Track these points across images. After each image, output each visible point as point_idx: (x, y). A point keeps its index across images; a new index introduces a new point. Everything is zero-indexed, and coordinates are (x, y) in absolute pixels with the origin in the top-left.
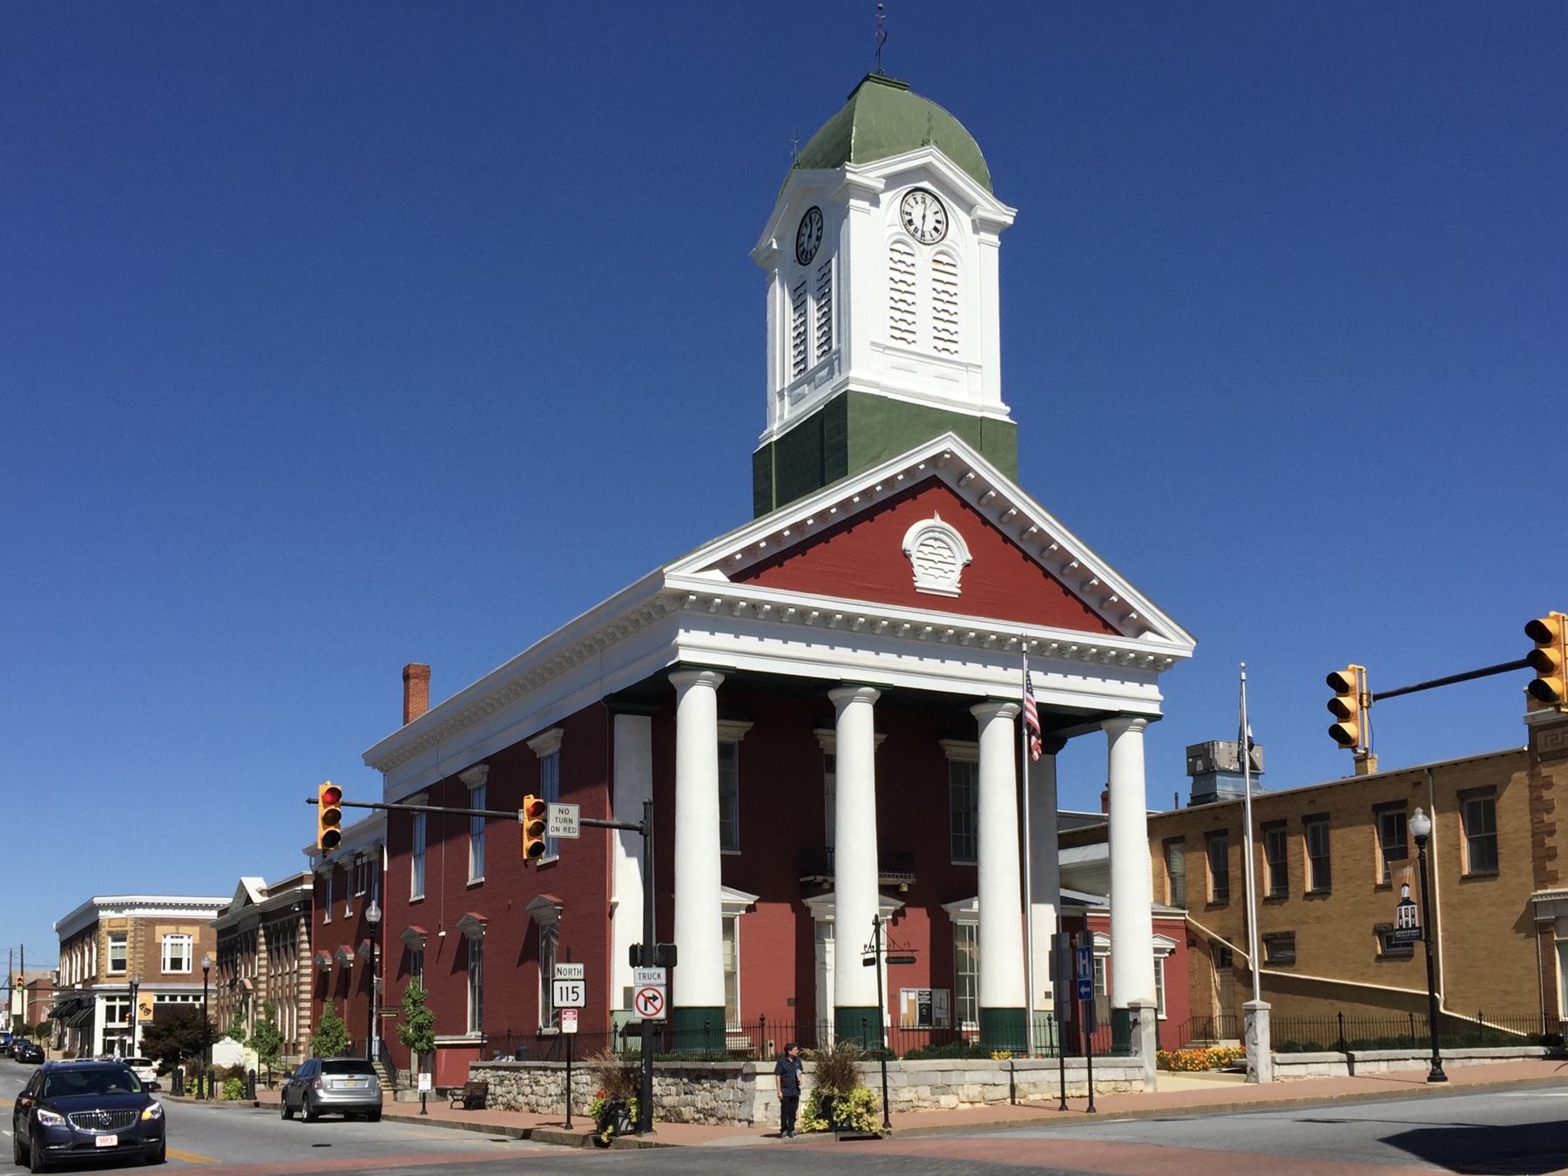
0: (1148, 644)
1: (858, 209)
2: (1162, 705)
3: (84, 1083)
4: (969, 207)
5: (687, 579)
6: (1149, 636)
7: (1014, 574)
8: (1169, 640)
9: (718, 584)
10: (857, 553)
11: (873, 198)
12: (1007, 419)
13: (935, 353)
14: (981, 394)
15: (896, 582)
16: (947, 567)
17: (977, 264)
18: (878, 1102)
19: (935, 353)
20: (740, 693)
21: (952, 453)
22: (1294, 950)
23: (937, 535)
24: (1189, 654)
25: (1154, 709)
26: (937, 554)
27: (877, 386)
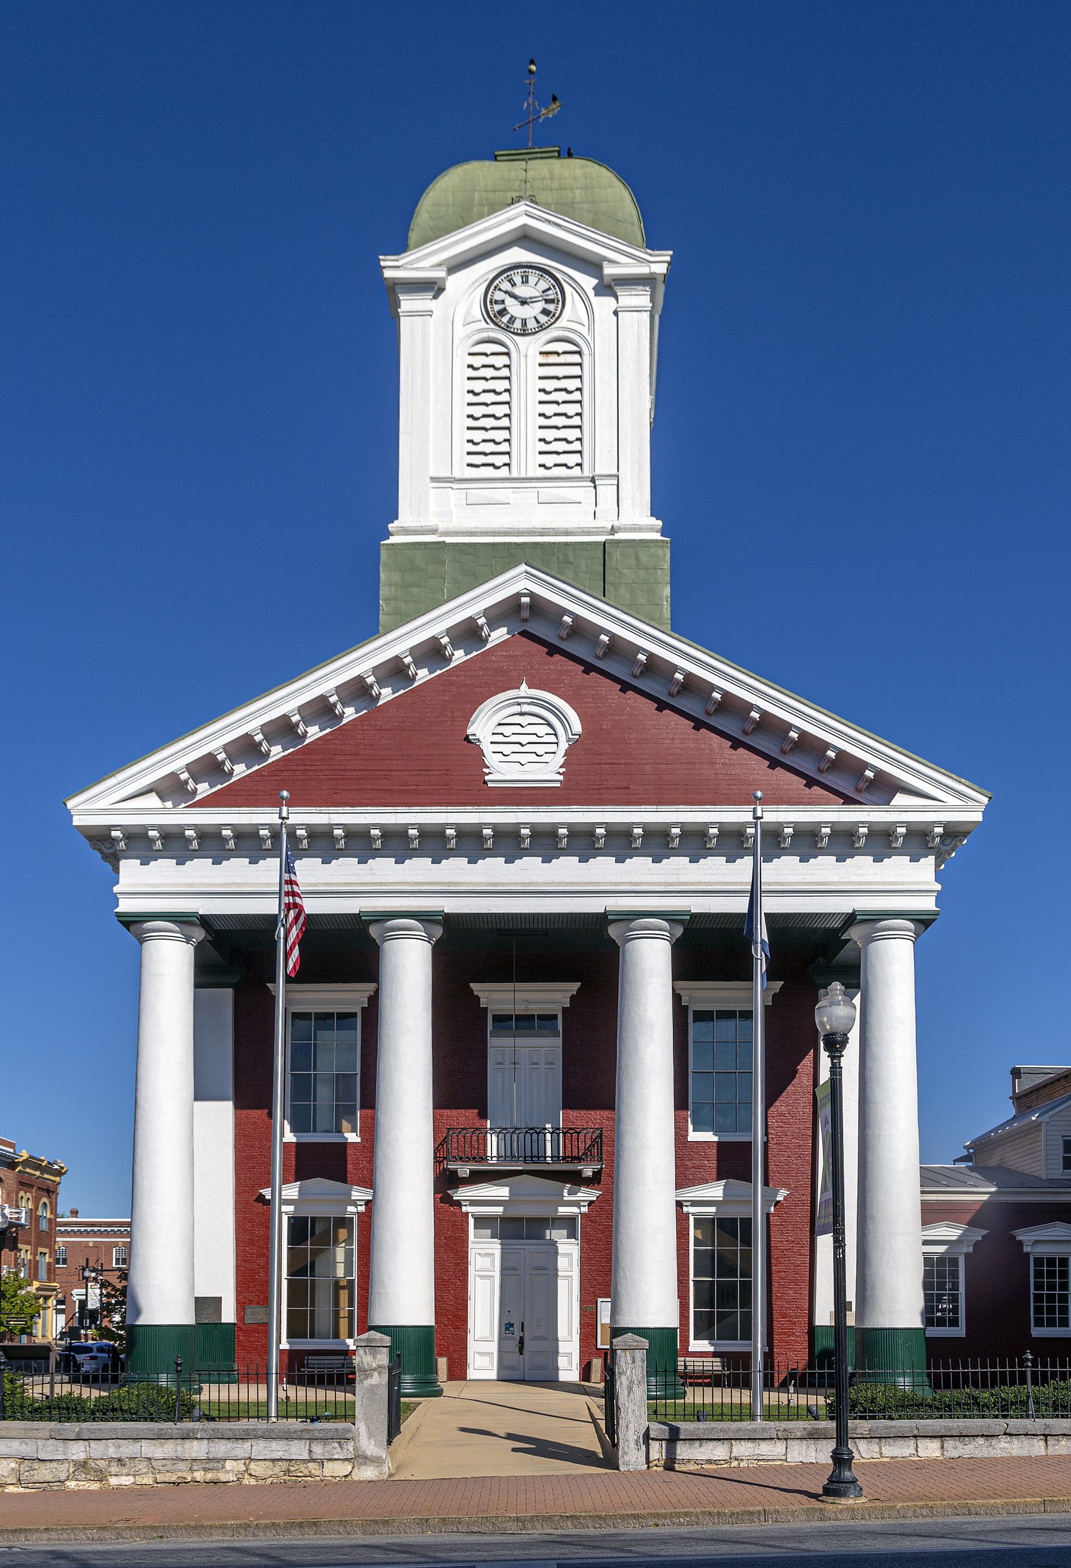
0: (901, 812)
1: (412, 314)
2: (940, 898)
3: (644, 1447)
4: (591, 265)
5: (104, 811)
6: (900, 799)
7: (647, 734)
8: (948, 800)
9: (156, 814)
10: (407, 751)
11: (434, 288)
12: (657, 536)
13: (542, 472)
14: (627, 510)
15: (465, 779)
16: (540, 749)
17: (618, 342)
18: (284, 1465)
19: (542, 472)
20: (232, 955)
21: (531, 595)
22: (924, 1203)
23: (526, 708)
24: (978, 817)
25: (928, 904)
26: (522, 738)
27: (434, 531)
